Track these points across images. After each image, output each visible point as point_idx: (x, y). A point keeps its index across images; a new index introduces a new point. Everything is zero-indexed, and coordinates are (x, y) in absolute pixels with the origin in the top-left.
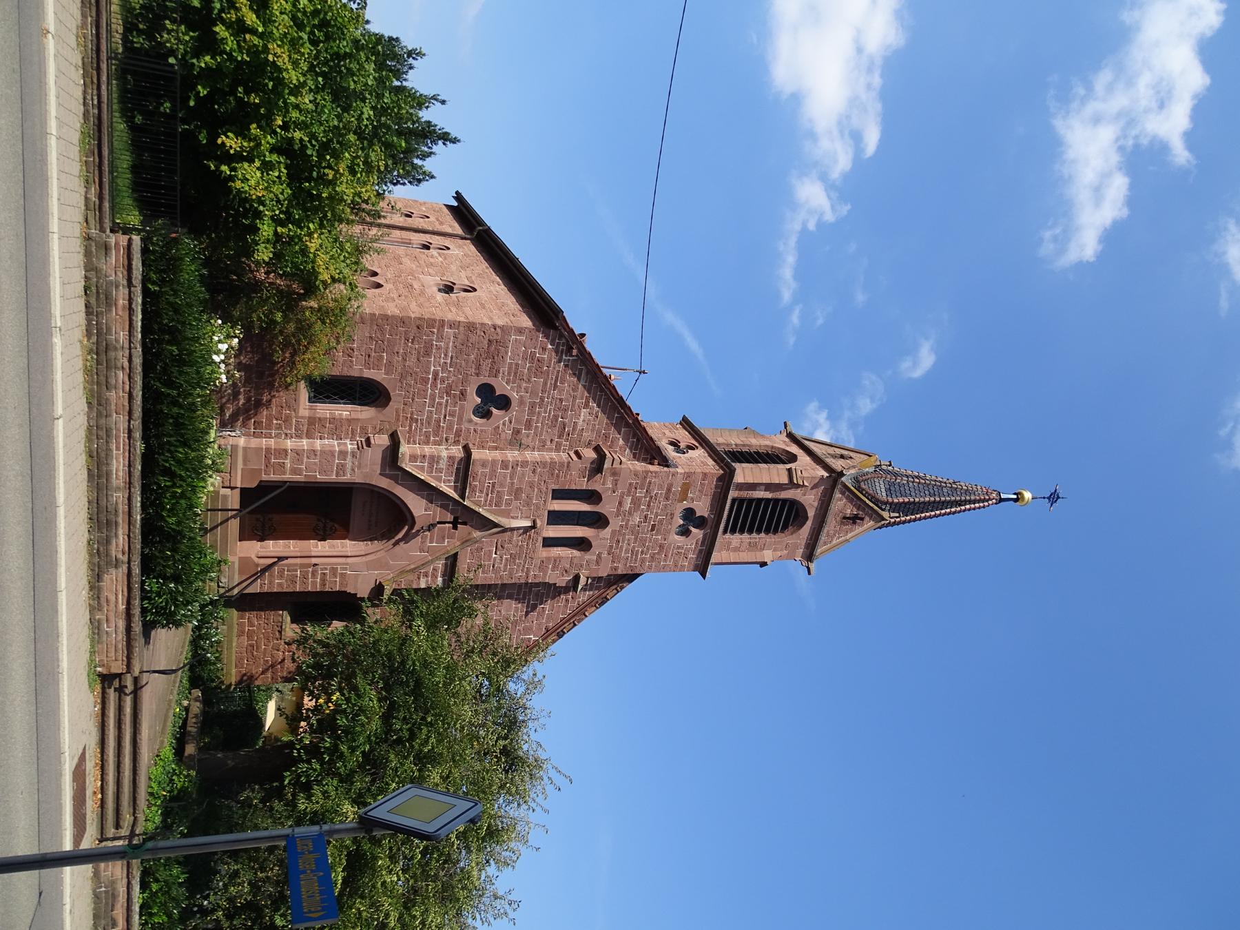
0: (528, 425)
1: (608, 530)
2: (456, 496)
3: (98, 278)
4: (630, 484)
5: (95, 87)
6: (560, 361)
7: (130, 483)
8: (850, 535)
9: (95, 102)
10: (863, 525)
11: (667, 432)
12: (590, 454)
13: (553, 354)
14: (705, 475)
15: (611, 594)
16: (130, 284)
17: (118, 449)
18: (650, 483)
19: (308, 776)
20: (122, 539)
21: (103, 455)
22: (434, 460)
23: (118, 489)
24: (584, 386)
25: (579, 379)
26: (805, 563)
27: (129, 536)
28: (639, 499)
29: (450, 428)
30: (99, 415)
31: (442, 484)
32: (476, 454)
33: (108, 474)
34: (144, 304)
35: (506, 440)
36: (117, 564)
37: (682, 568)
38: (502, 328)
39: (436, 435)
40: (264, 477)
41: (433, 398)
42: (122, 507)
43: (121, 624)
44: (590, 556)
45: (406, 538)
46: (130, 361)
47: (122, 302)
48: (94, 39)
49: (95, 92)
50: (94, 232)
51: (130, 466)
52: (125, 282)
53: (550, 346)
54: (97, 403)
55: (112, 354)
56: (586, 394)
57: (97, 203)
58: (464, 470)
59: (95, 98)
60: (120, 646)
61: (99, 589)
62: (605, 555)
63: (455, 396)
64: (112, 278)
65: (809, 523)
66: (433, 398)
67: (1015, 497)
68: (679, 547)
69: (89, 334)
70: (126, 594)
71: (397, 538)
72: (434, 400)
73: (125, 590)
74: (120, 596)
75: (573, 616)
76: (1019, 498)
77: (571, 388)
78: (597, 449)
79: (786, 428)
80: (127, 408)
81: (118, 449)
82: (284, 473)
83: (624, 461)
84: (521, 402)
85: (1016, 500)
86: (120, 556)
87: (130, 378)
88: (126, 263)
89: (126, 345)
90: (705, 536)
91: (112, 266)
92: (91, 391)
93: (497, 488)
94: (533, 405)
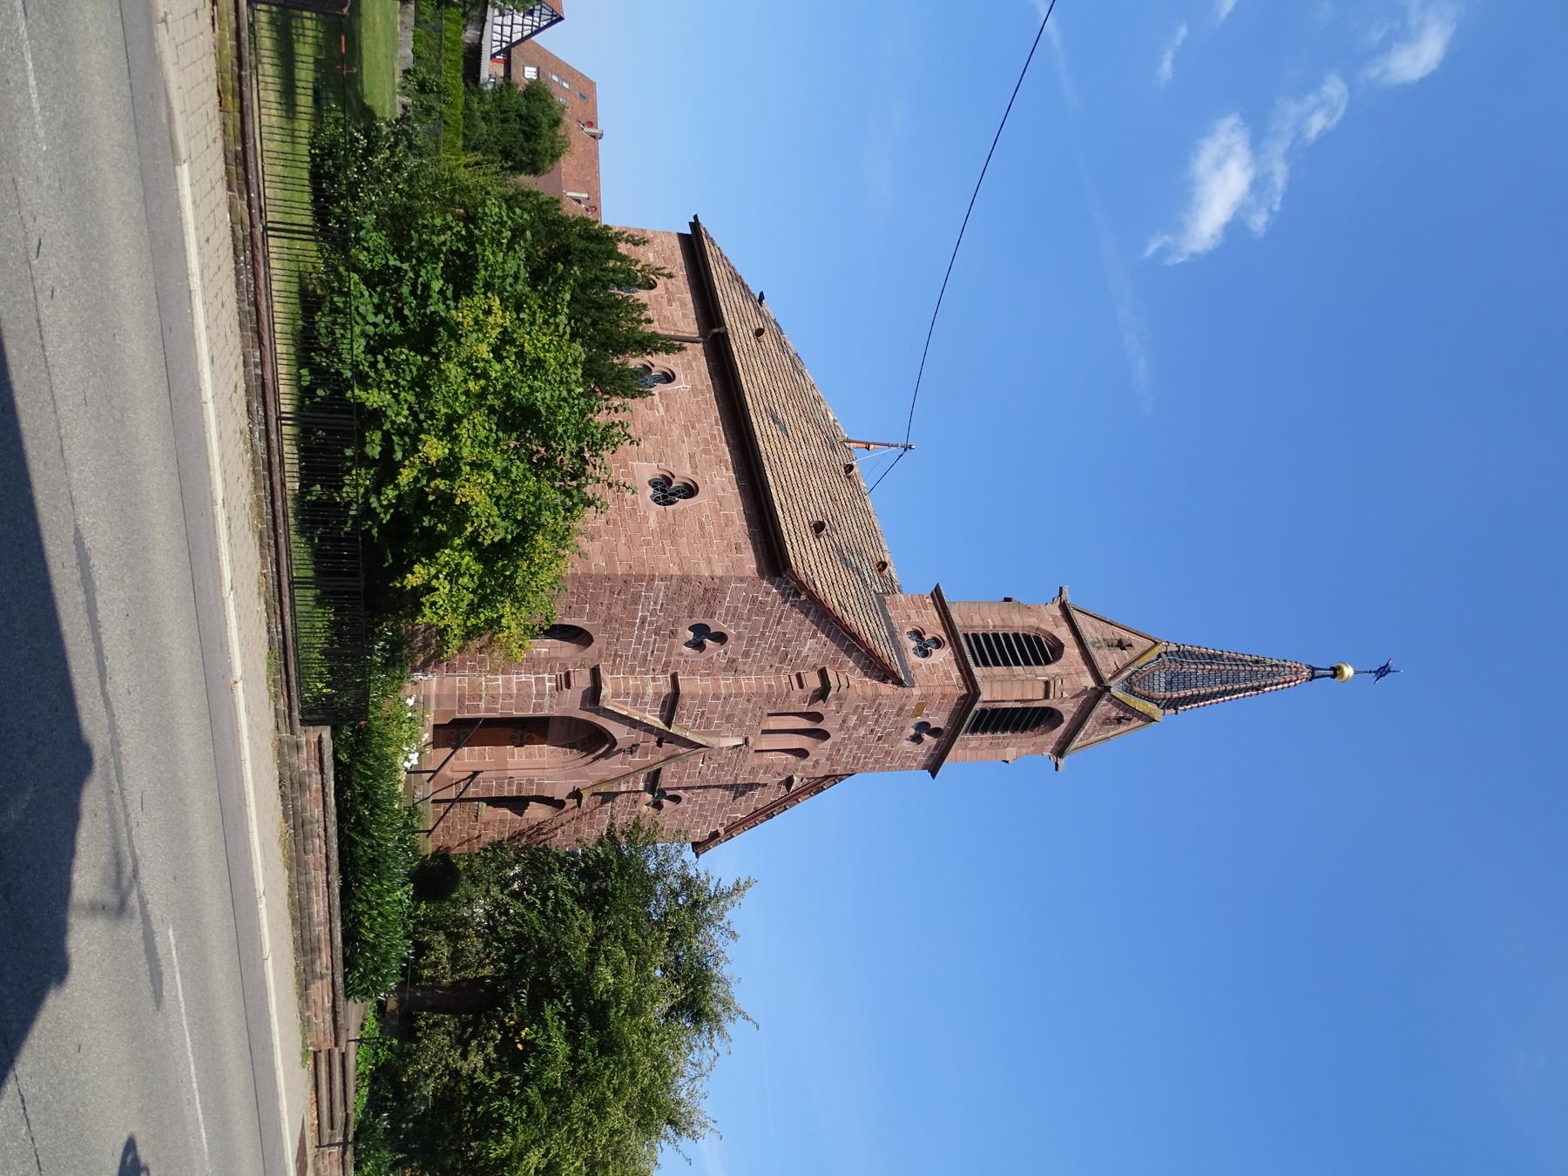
0: (746, 654)
1: (829, 742)
2: (661, 725)
3: (292, 772)
4: (857, 706)
5: (278, 617)
6: (785, 602)
7: (330, 920)
8: (1111, 733)
9: (280, 629)
10: (1129, 724)
11: (912, 613)
12: (813, 682)
13: (779, 597)
14: (944, 696)
15: (828, 785)
16: (322, 771)
17: (318, 895)
18: (880, 704)
19: (499, 960)
20: (325, 957)
21: (304, 902)
22: (638, 697)
23: (319, 924)
24: (812, 621)
25: (807, 616)
26: (1053, 758)
27: (331, 957)
28: (866, 718)
29: (658, 660)
30: (299, 874)
31: (647, 715)
32: (684, 688)
33: (310, 917)
34: (336, 776)
35: (720, 667)
36: (322, 977)
37: (910, 768)
38: (721, 578)
39: (640, 666)
40: (458, 716)
41: (639, 639)
42: (325, 937)
43: (329, 1017)
44: (808, 762)
45: (606, 755)
46: (325, 830)
47: (315, 783)
48: (275, 576)
49: (279, 621)
50: (285, 735)
51: (329, 907)
52: (318, 770)
53: (775, 591)
54: (296, 864)
55: (308, 828)
56: (814, 627)
57: (287, 711)
58: (670, 706)
59: (279, 626)
60: (328, 1031)
61: (307, 996)
62: (823, 760)
63: (664, 635)
64: (305, 769)
65: (1063, 726)
66: (639, 639)
67: (1331, 672)
68: (907, 752)
69: (286, 817)
70: (331, 996)
71: (597, 753)
72: (641, 640)
73: (331, 993)
74: (326, 998)
75: (787, 800)
76: (1336, 672)
77: (796, 622)
78: (823, 674)
79: (1060, 595)
80: (325, 865)
81: (318, 895)
82: (479, 712)
83: (852, 680)
84: (739, 637)
85: (1334, 676)
86: (324, 971)
87: (326, 844)
88: (318, 755)
89: (322, 819)
90: (938, 744)
91: (304, 761)
92: (290, 858)
93: (707, 715)
94: (751, 640)
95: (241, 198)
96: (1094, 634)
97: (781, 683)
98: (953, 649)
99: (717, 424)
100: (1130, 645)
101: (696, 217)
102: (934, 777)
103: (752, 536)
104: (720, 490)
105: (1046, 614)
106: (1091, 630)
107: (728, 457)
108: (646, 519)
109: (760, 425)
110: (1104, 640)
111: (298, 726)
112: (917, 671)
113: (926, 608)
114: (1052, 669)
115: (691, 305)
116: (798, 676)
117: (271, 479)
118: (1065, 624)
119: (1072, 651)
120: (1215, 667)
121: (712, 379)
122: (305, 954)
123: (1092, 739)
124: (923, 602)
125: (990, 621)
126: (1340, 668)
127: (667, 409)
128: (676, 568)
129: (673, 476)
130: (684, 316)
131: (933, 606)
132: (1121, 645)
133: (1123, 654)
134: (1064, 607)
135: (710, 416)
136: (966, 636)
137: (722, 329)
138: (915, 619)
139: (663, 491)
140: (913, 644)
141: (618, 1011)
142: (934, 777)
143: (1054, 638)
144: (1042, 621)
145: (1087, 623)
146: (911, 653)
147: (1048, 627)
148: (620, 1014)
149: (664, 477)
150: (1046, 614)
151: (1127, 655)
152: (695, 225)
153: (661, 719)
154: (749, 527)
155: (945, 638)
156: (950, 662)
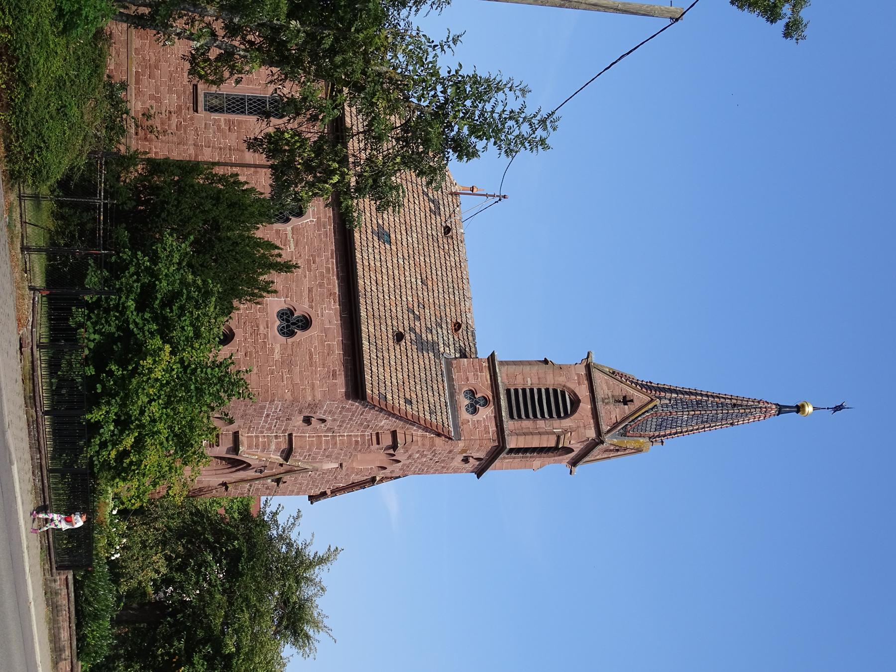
11: (471, 375)
16: (68, 588)
20: (67, 653)
33: (60, 639)
46: (69, 608)
50: (48, 576)
52: (65, 588)
69: (48, 605)
70: (70, 666)
76: (799, 409)
79: (588, 357)
85: (798, 412)
89: (67, 604)
95: (32, 408)
96: (606, 391)
98: (495, 408)
99: (332, 258)
100: (632, 401)
102: (478, 477)
103: (345, 364)
105: (573, 372)
106: (605, 388)
107: (337, 291)
108: (272, 350)
110: (613, 396)
111: (54, 570)
112: (465, 426)
113: (481, 371)
114: (567, 423)
116: (377, 434)
117: (44, 494)
118: (586, 382)
119: (585, 407)
122: (56, 651)
123: (598, 457)
124: (481, 365)
125: (529, 379)
126: (803, 406)
127: (296, 245)
128: (289, 393)
129: (295, 310)
131: (487, 369)
132: (626, 401)
133: (624, 409)
134: (588, 367)
135: (328, 250)
136: (508, 391)
138: (472, 381)
139: (288, 321)
140: (467, 402)
141: (238, 660)
142: (478, 477)
143: (575, 394)
144: (568, 379)
145: (604, 382)
146: (463, 409)
148: (239, 662)
150: (573, 372)
151: (627, 409)
153: (281, 456)
154: (344, 355)
155: (491, 398)
156: (490, 419)
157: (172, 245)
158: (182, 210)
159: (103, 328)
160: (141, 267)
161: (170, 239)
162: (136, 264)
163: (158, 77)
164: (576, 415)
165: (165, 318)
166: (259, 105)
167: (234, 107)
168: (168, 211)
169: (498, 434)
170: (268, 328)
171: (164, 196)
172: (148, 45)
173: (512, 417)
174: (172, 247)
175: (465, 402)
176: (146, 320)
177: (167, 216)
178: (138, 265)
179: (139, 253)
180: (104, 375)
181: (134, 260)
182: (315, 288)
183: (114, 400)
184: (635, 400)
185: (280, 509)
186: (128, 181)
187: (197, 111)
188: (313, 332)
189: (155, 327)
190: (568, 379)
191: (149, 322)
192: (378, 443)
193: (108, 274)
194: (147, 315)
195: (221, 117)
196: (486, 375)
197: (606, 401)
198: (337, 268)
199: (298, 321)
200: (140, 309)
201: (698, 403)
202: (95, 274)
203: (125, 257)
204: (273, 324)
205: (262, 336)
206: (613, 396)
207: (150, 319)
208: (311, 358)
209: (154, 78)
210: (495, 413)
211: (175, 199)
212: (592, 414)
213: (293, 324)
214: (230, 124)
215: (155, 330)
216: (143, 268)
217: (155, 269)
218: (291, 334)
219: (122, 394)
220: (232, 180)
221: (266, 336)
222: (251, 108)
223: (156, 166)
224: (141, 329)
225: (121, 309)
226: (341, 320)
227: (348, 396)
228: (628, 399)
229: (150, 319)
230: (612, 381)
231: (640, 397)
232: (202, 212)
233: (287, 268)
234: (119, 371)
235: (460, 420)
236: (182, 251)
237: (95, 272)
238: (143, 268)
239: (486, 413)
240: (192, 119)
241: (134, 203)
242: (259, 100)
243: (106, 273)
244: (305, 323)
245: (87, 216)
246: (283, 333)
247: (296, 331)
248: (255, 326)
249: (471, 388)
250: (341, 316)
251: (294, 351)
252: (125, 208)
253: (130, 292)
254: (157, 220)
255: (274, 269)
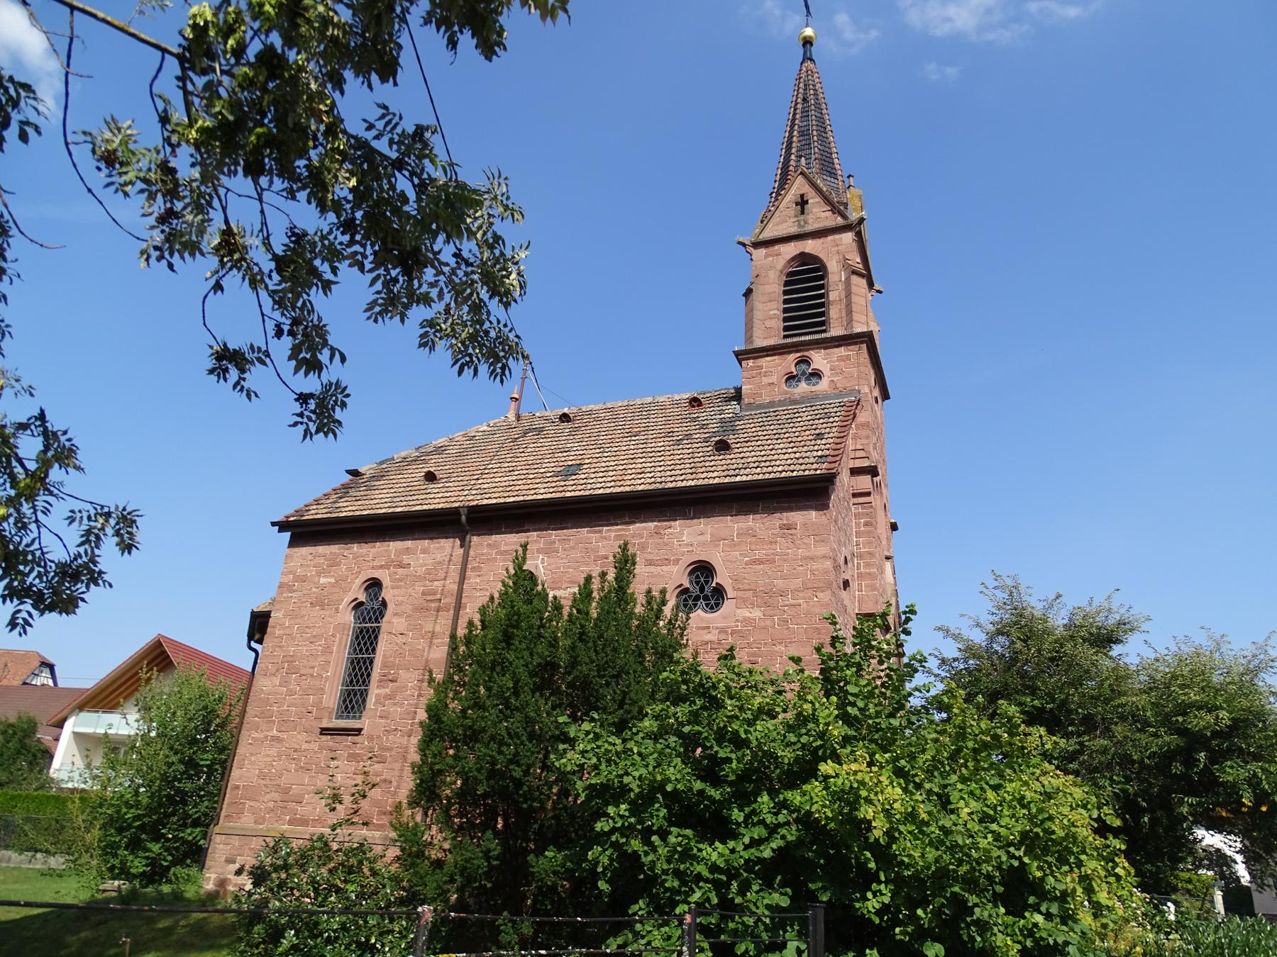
11: (765, 380)
76: (807, 42)
85: (811, 44)
96: (789, 224)
97: (863, 514)
98: (812, 349)
99: (600, 532)
101: (273, 524)
103: (771, 511)
104: (701, 538)
106: (785, 225)
107: (652, 525)
109: (572, 490)
112: (838, 385)
113: (760, 367)
115: (409, 543)
116: (855, 495)
118: (776, 247)
119: (810, 246)
120: (815, 133)
121: (528, 531)
126: (805, 38)
128: (820, 595)
129: (356, 599)
130: (424, 551)
132: (802, 203)
134: (757, 245)
136: (785, 337)
137: (461, 510)
139: (697, 598)
143: (793, 259)
145: (776, 228)
146: (813, 388)
147: (781, 263)
149: (355, 608)
151: (814, 200)
152: (283, 526)
154: (755, 513)
155: (799, 355)
156: (828, 354)
157: (583, 752)
158: (509, 734)
159: (764, 923)
160: (630, 824)
161: (569, 755)
162: (623, 835)
163: (302, 790)
164: (822, 256)
165: (743, 777)
166: (365, 644)
167: (362, 675)
168: (511, 762)
169: (850, 344)
170: (709, 628)
171: (479, 770)
172: (252, 804)
173: (824, 331)
174: (587, 752)
175: (803, 387)
176: (747, 817)
177: (519, 766)
178: (627, 831)
179: (598, 826)
180: (897, 930)
181: (614, 838)
182: (646, 556)
183: (977, 910)
184: (801, 192)
185: (937, 654)
186: (446, 846)
187: (360, 730)
188: (716, 559)
189: (766, 798)
190: (772, 267)
191: (754, 812)
192: (868, 494)
193: (641, 902)
194: (738, 815)
195: (374, 691)
196: (766, 362)
197: (802, 223)
198: (617, 525)
199: (697, 583)
200: (719, 829)
201: (802, 134)
202: (643, 937)
203: (606, 861)
204: (702, 619)
205: (723, 636)
206: (796, 216)
207: (747, 810)
208: (760, 562)
209: (302, 796)
210: (821, 348)
211: (487, 747)
212: (820, 238)
213: (702, 590)
214: (388, 679)
215: (772, 799)
216: (632, 820)
217: (637, 790)
218: (719, 593)
219: (956, 889)
220: (462, 649)
221: (723, 630)
222: (367, 650)
223: (426, 792)
224: (773, 830)
225: (723, 877)
226: (699, 518)
227: (823, 506)
228: (799, 200)
229: (747, 810)
230: (776, 219)
231: (798, 186)
232: (516, 694)
233: (626, 561)
234: (880, 891)
235: (830, 391)
236: (598, 730)
237: (637, 935)
238: (632, 820)
239: (819, 359)
240: (371, 738)
241: (489, 834)
242: (357, 638)
243: (639, 907)
244: (702, 570)
245: (507, 934)
246: (717, 605)
247: (714, 585)
248: (705, 647)
249: (784, 380)
250: (692, 519)
251: (749, 587)
252: (496, 853)
253: (686, 855)
254: (525, 788)
255: (629, 583)
